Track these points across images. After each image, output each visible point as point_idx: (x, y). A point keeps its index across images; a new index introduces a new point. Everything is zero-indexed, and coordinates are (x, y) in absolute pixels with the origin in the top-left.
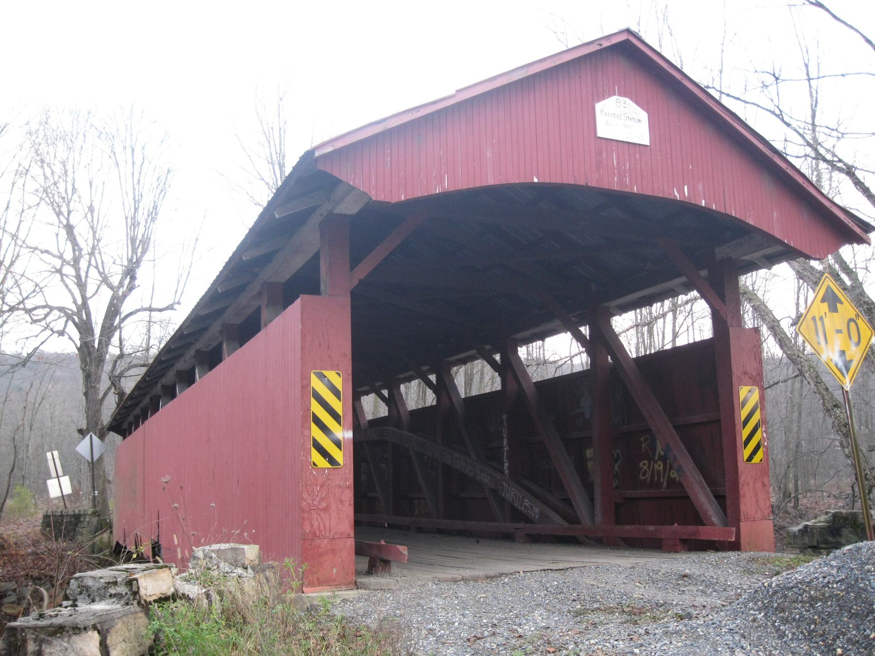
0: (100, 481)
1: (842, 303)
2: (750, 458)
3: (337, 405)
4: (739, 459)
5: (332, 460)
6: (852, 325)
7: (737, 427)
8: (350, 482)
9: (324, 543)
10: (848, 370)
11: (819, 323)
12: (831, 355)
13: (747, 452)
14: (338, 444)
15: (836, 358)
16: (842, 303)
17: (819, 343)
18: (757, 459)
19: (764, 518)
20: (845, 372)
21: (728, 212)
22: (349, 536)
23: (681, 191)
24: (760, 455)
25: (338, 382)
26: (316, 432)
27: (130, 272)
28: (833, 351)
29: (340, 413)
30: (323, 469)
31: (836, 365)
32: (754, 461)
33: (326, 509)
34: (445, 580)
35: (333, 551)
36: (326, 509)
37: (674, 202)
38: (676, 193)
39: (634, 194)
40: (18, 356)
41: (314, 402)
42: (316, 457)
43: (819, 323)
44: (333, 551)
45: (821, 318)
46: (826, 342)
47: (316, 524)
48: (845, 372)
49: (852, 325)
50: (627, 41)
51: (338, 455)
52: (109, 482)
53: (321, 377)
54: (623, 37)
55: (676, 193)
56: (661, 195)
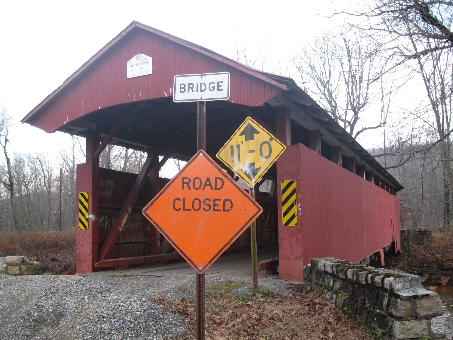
1: (258, 133)
2: (287, 223)
3: (87, 205)
5: (85, 227)
7: (278, 206)
9: (82, 257)
10: (254, 175)
11: (235, 149)
12: (242, 167)
13: (285, 220)
14: (87, 220)
16: (258, 133)
17: (233, 161)
18: (292, 224)
19: (296, 259)
20: (252, 176)
24: (295, 221)
25: (87, 196)
27: (74, 159)
29: (88, 208)
30: (82, 230)
31: (245, 173)
32: (290, 225)
34: (120, 276)
35: (85, 261)
36: (83, 245)
38: (165, 94)
39: (144, 101)
40: (432, 143)
43: (235, 149)
45: (238, 146)
46: (239, 159)
47: (80, 250)
48: (252, 176)
53: (82, 194)
54: (133, 26)
55: (165, 94)
56: (157, 97)
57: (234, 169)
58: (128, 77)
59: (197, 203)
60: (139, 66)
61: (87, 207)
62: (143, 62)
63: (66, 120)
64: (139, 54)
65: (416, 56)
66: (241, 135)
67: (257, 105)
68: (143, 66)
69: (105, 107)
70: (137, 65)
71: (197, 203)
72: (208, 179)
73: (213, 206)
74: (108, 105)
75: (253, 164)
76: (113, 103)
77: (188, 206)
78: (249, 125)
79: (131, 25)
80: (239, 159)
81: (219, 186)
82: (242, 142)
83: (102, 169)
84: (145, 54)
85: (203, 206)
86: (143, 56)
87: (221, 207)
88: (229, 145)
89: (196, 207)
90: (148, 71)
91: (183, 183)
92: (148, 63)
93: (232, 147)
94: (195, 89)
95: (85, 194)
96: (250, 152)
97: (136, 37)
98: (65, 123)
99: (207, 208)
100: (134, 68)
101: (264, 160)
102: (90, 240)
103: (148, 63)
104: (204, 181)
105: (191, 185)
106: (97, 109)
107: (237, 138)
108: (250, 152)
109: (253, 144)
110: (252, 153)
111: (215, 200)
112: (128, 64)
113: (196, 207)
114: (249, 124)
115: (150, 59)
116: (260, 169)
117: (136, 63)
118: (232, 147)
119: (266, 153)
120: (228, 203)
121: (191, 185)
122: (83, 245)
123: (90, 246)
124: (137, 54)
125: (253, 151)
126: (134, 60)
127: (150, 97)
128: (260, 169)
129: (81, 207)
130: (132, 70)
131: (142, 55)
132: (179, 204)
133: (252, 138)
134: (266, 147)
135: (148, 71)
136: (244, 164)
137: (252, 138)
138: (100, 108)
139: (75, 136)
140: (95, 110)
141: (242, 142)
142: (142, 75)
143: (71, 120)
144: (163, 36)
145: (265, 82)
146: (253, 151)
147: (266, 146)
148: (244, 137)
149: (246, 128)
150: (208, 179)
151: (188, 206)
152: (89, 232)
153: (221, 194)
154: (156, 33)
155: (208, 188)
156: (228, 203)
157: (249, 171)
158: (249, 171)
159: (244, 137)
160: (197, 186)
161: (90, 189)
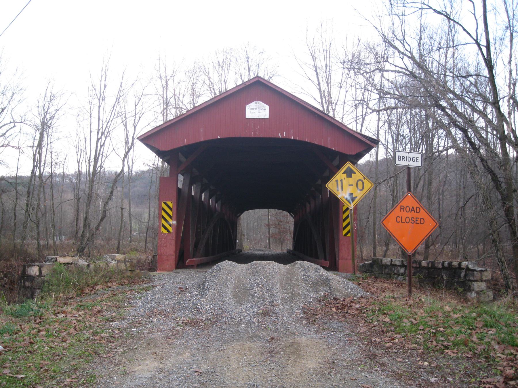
0: (240, 235)
2: (346, 234)
3: (171, 213)
4: (340, 234)
5: (168, 231)
6: (360, 183)
8: (174, 238)
9: (165, 257)
10: (353, 201)
11: (339, 183)
12: (344, 195)
13: (344, 232)
14: (170, 225)
15: (347, 196)
17: (338, 191)
20: (351, 201)
21: (304, 140)
22: (173, 255)
23: (282, 134)
25: (171, 205)
26: (163, 222)
28: (346, 193)
31: (346, 199)
33: (166, 246)
37: (279, 139)
41: (163, 212)
42: (163, 229)
43: (339, 183)
44: (168, 260)
45: (341, 181)
46: (342, 190)
48: (351, 201)
49: (360, 183)
50: (258, 80)
51: (170, 229)
52: (244, 235)
53: (166, 204)
58: (247, 117)
59: (407, 219)
60: (257, 111)
61: (171, 215)
65: (378, 111)
66: (343, 173)
68: (261, 111)
70: (256, 109)
71: (407, 219)
72: (413, 207)
73: (415, 221)
75: (352, 194)
77: (404, 220)
78: (349, 167)
80: (342, 190)
81: (418, 211)
85: (410, 220)
87: (419, 222)
88: (335, 179)
89: (408, 221)
90: (265, 115)
91: (401, 209)
92: (265, 109)
93: (337, 181)
94: (405, 159)
95: (169, 203)
96: (350, 185)
97: (258, 88)
99: (413, 222)
100: (252, 111)
101: (359, 192)
102: (173, 242)
103: (265, 109)
104: (411, 208)
105: (405, 209)
106: (216, 138)
107: (340, 175)
108: (350, 185)
109: (352, 180)
110: (351, 187)
111: (416, 218)
112: (247, 107)
113: (408, 221)
114: (349, 167)
115: (267, 107)
116: (356, 197)
117: (255, 108)
118: (337, 181)
119: (360, 187)
120: (422, 220)
121: (405, 209)
122: (166, 246)
123: (173, 247)
125: (352, 185)
127: (267, 136)
128: (356, 197)
129: (163, 214)
130: (250, 112)
132: (399, 219)
133: (351, 176)
134: (360, 183)
135: (265, 115)
136: (346, 193)
137: (351, 176)
144: (283, 92)
145: (361, 140)
146: (352, 185)
147: (360, 183)
148: (346, 174)
149: (347, 169)
150: (413, 207)
151: (404, 220)
152: (173, 236)
153: (419, 215)
155: (413, 212)
156: (422, 220)
157: (349, 198)
158: (349, 198)
159: (346, 174)
160: (408, 210)
161: (175, 199)
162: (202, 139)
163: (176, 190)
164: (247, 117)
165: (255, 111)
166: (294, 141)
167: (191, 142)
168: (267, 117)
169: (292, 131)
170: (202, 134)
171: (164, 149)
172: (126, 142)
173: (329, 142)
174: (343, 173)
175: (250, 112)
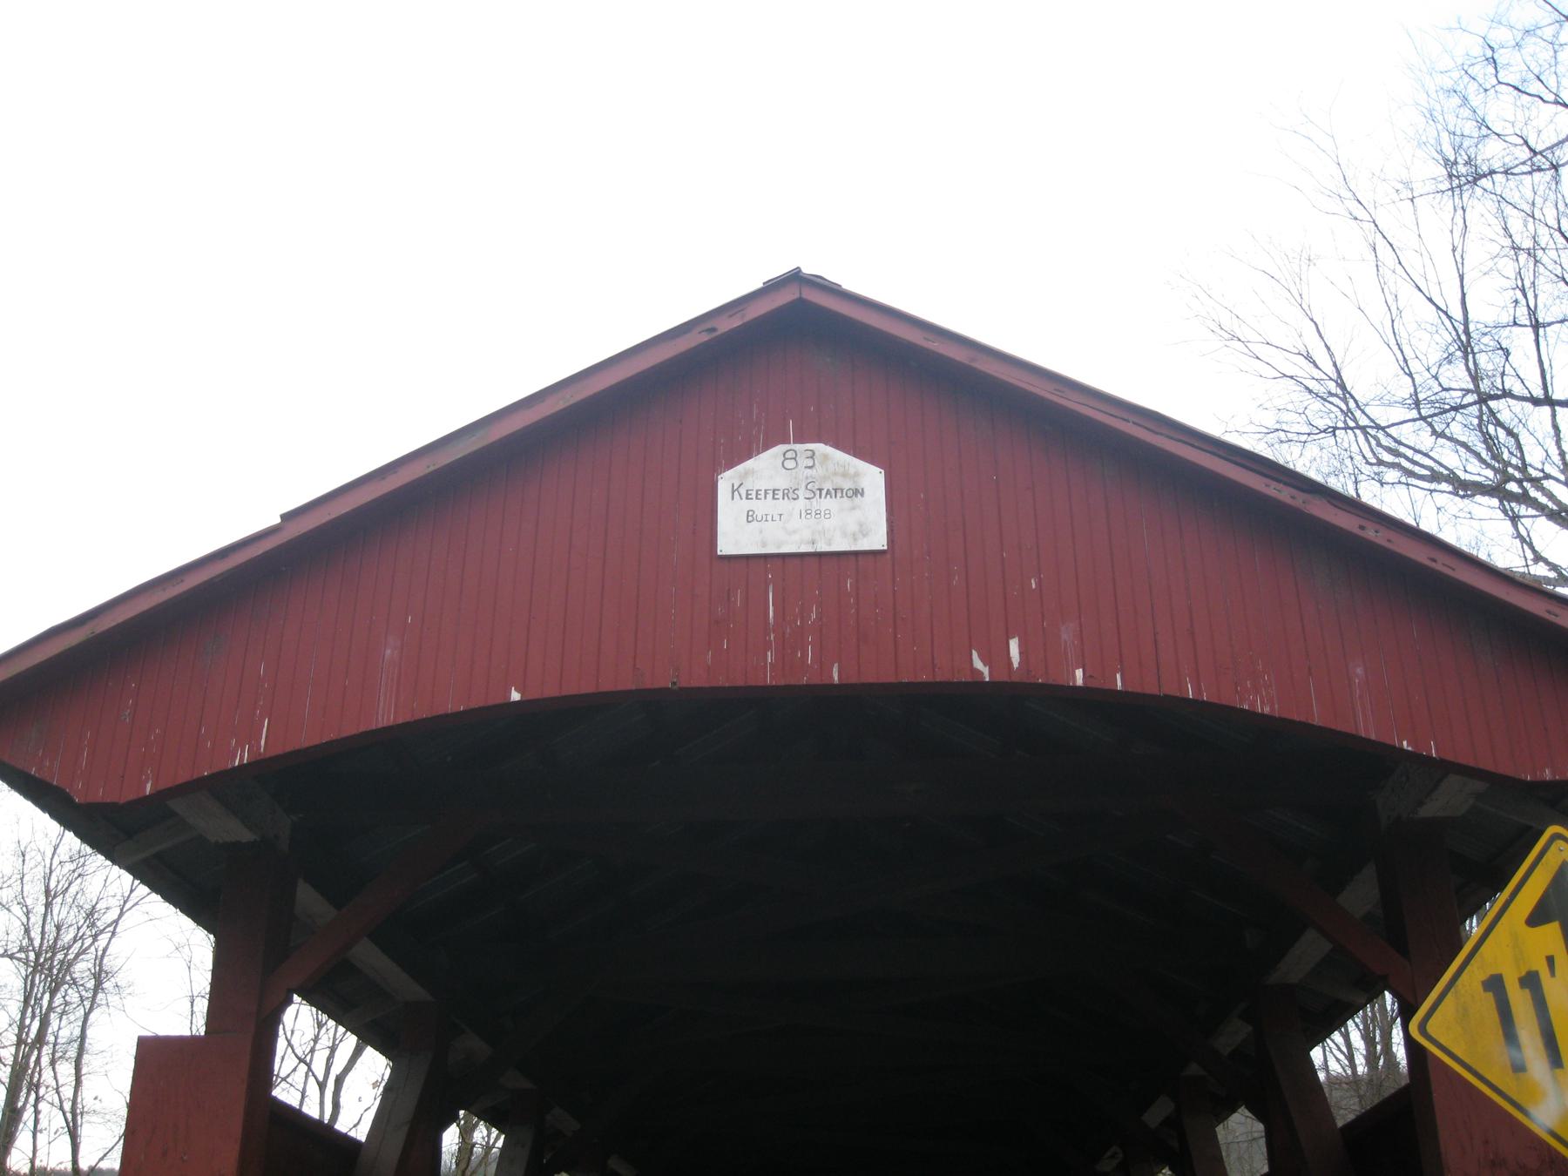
11: (1520, 1001)
17: (1519, 1068)
23: (996, 655)
38: (978, 664)
43: (1520, 1001)
45: (1531, 981)
46: (1555, 1059)
55: (978, 664)
57: (1533, 1111)
58: (726, 546)
60: (800, 503)
62: (827, 486)
63: (254, 737)
64: (800, 439)
66: (1537, 917)
67: (1548, 775)
68: (827, 503)
69: (551, 691)
70: (790, 494)
74: (579, 684)
76: (616, 677)
79: (772, 287)
82: (1550, 961)
83: (291, 1118)
84: (837, 446)
86: (826, 457)
88: (1474, 977)
90: (864, 531)
92: (858, 492)
93: (1495, 984)
97: (792, 352)
98: (242, 757)
100: (761, 507)
103: (858, 492)
112: (725, 481)
115: (873, 479)
117: (782, 482)
118: (1495, 984)
124: (786, 441)
126: (766, 467)
130: (750, 517)
131: (820, 448)
138: (515, 696)
139: (127, 878)
140: (477, 702)
141: (1550, 961)
142: (822, 547)
143: (278, 751)
148: (1552, 930)
154: (936, 346)
162: (386, 714)
163: (236, 1125)
164: (726, 546)
165: (783, 505)
166: (1094, 701)
167: (308, 736)
168: (877, 539)
169: (1067, 634)
170: (388, 675)
171: (100, 795)
172: (114, 933)
173: (1361, 689)
174: (1537, 917)
175: (750, 517)
